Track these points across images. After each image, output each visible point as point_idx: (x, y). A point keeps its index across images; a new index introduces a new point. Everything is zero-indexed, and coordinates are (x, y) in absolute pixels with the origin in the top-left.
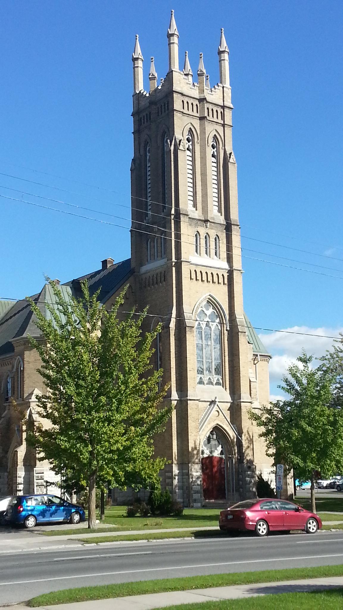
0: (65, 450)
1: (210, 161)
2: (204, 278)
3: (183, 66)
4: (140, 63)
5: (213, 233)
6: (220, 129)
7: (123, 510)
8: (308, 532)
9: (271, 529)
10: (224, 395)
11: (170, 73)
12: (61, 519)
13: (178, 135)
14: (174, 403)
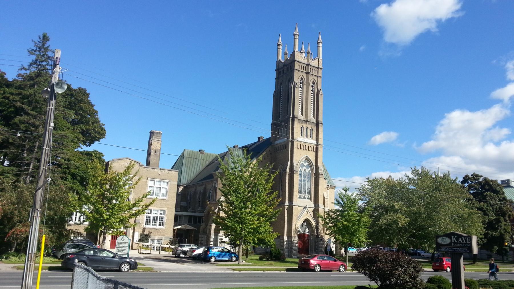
0: (229, 227)
1: (311, 94)
2: (304, 148)
3: (300, 48)
4: (281, 47)
5: (310, 127)
6: (316, 78)
7: (257, 257)
8: (340, 271)
9: (322, 269)
10: (311, 204)
11: (293, 53)
12: (227, 259)
13: (296, 81)
14: (287, 207)
